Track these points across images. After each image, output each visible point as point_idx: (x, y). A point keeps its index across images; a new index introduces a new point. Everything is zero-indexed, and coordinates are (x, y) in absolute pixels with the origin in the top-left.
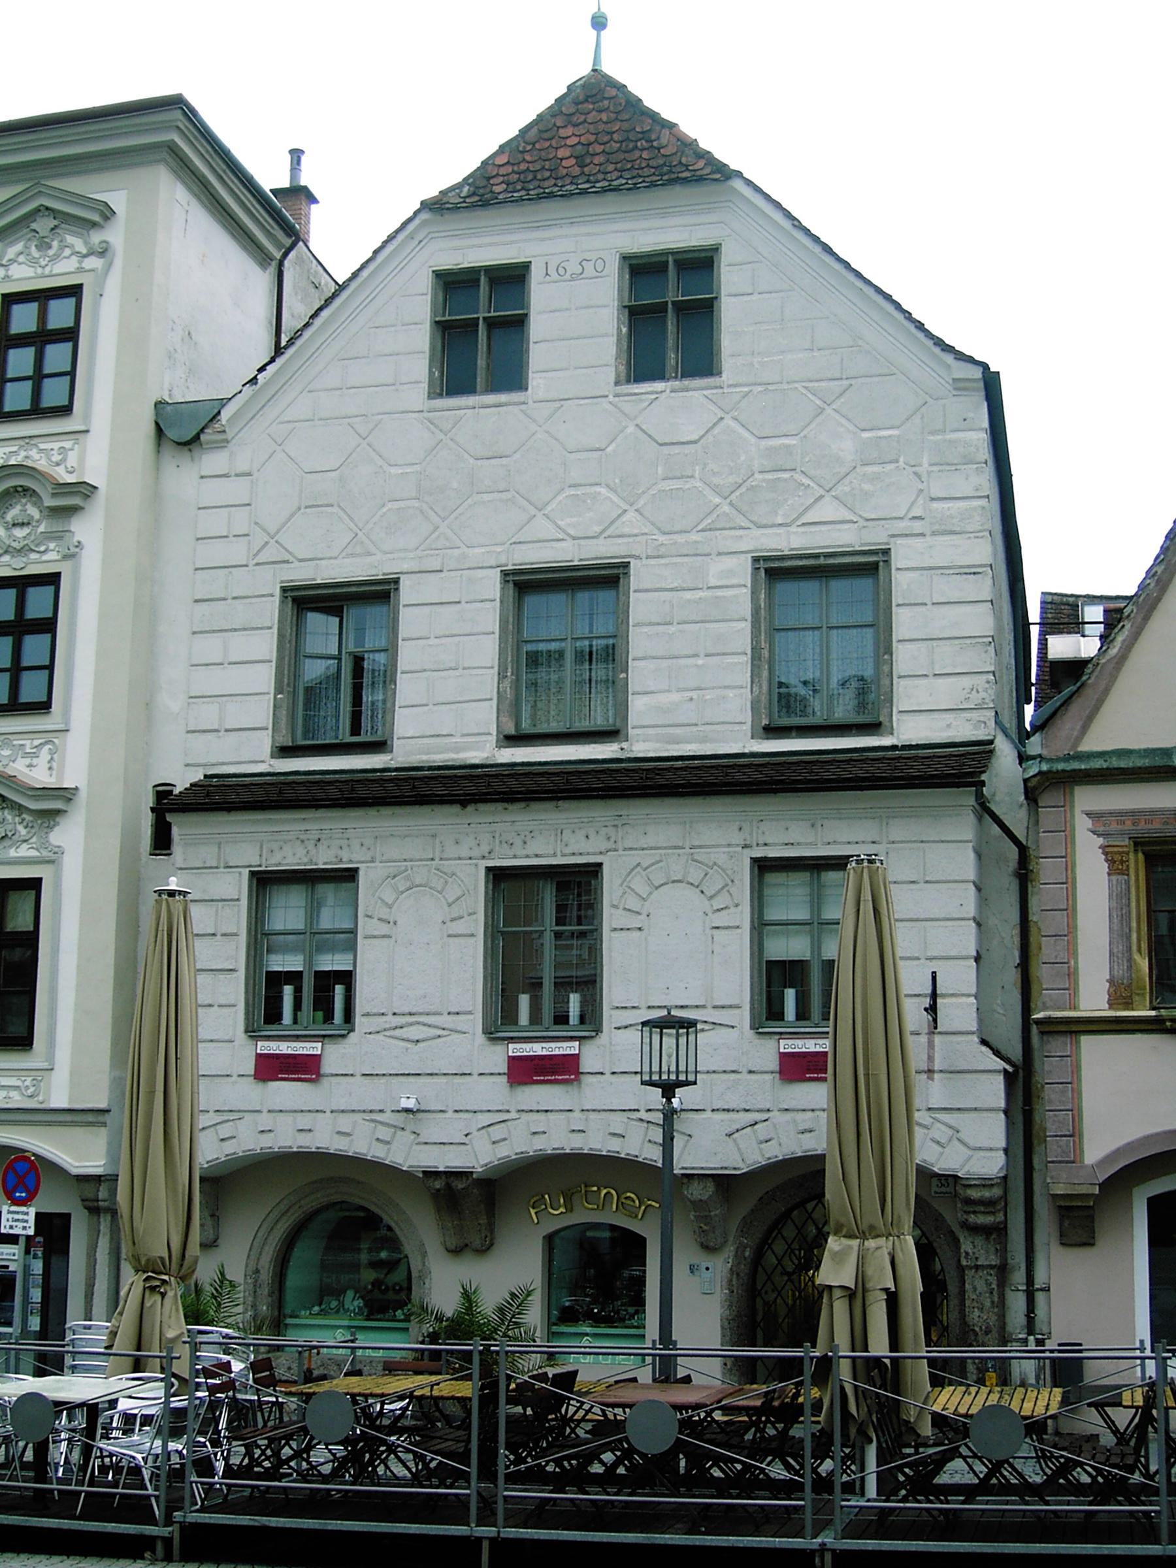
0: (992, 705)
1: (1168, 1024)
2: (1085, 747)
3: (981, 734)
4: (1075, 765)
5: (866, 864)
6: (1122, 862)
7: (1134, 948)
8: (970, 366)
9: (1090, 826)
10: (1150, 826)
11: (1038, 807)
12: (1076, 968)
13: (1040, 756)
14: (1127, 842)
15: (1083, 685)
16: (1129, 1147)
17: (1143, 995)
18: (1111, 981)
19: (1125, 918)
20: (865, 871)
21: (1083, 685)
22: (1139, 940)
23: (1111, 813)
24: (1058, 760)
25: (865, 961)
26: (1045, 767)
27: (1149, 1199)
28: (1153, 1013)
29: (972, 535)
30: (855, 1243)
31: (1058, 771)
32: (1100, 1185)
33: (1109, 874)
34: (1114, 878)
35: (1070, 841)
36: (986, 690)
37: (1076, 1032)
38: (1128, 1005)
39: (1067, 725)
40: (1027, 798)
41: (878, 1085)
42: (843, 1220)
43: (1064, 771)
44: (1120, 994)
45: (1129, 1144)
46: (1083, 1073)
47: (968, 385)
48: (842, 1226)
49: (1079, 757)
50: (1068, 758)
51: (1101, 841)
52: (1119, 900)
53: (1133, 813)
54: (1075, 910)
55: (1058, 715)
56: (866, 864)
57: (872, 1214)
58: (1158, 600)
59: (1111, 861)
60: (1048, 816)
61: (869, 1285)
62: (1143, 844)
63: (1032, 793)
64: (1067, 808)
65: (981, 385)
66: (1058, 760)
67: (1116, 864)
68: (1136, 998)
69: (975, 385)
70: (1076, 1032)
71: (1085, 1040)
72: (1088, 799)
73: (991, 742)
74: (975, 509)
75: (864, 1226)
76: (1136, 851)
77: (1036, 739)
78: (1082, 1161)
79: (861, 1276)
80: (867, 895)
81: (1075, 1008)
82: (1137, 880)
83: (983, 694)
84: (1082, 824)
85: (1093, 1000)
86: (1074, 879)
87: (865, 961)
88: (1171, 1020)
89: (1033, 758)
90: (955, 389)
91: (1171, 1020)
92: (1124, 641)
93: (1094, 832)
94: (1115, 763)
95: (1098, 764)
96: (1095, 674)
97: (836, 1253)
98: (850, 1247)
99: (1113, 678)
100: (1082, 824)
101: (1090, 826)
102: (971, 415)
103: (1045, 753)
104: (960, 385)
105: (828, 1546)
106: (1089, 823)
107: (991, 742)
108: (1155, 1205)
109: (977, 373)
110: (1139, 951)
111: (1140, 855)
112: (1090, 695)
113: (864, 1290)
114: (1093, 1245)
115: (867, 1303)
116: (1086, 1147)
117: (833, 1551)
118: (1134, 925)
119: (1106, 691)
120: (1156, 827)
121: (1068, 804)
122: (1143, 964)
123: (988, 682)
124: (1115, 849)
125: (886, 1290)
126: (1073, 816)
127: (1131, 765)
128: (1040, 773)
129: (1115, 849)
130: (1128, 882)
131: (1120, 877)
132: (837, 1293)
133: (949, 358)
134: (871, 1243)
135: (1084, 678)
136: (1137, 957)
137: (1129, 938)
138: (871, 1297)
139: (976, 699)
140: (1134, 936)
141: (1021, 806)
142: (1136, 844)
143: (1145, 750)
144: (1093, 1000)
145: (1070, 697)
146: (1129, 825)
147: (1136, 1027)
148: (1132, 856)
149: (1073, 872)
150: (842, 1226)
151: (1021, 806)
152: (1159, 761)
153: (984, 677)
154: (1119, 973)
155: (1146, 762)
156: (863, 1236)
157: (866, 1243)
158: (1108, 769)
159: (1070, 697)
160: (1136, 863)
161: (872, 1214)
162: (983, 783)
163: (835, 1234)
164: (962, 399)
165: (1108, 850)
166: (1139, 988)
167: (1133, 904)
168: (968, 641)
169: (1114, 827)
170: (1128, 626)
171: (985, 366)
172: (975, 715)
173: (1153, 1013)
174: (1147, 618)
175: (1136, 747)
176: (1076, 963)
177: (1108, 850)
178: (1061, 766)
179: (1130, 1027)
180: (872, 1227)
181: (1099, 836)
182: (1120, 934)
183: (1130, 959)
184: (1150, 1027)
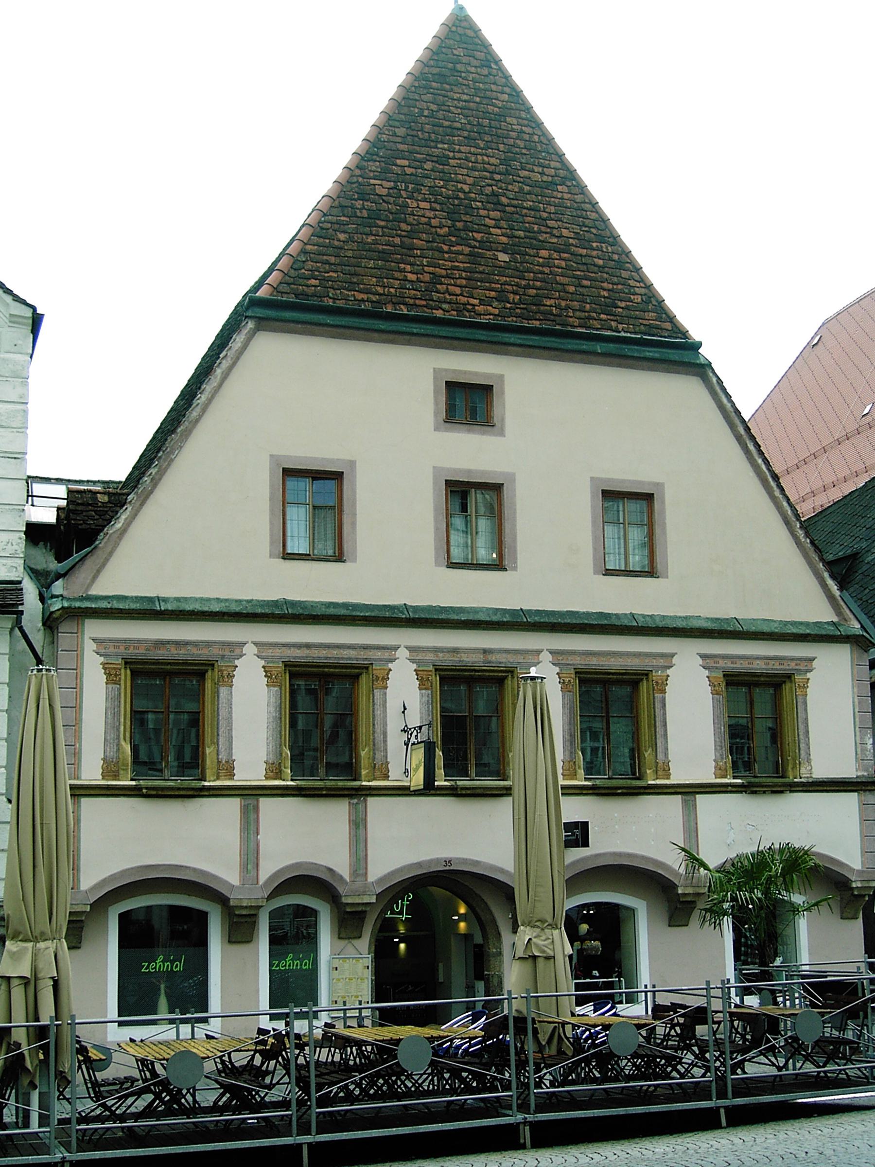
0: (22, 556)
1: (144, 791)
2: (94, 591)
3: (13, 576)
4: (87, 604)
5: (44, 672)
6: (116, 675)
7: (122, 736)
8: (23, 306)
9: (95, 649)
10: (137, 651)
11: (58, 632)
12: (80, 749)
13: (61, 596)
14: (120, 661)
15: (95, 547)
16: (113, 877)
17: (127, 769)
18: (104, 759)
19: (116, 715)
20: (44, 677)
21: (95, 547)
22: (125, 731)
23: (110, 640)
24: (75, 599)
25: (43, 742)
26: (66, 604)
27: (120, 915)
28: (133, 783)
29: (15, 430)
30: (30, 945)
31: (75, 608)
32: (91, 905)
33: (107, 684)
34: (110, 686)
35: (80, 658)
36: (18, 544)
37: (78, 795)
38: (116, 777)
39: (83, 574)
40: (44, 624)
41: (49, 831)
42: (21, 929)
43: (79, 608)
44: (111, 768)
45: (112, 875)
46: (82, 824)
47: (20, 320)
48: (20, 933)
49: (89, 598)
50: (82, 599)
51: (102, 659)
52: (113, 701)
53: (125, 641)
54: (81, 707)
55: (77, 567)
56: (44, 672)
57: (43, 924)
58: (151, 492)
59: (108, 675)
60: (65, 639)
61: (40, 976)
62: (131, 663)
63: (50, 623)
64: (79, 634)
65: (30, 321)
66: (75, 599)
67: (112, 676)
68: (121, 772)
69: (25, 321)
70: (78, 795)
71: (370, 800)
72: (94, 629)
73: (20, 582)
74: (18, 411)
75: (37, 933)
76: (126, 668)
77: (59, 583)
78: (78, 888)
79: (35, 970)
80: (45, 695)
81: (78, 778)
82: (126, 688)
83: (15, 547)
84: (90, 647)
85: (91, 773)
86: (82, 685)
87: (43, 742)
88: (146, 788)
89: (57, 596)
90: (10, 322)
91: (146, 788)
92: (126, 519)
93: (98, 653)
94: (116, 605)
95: (104, 605)
96: (105, 540)
97: (14, 953)
98: (26, 948)
99: (116, 545)
100: (90, 647)
101: (95, 649)
102: (20, 342)
103: (65, 594)
104: (14, 319)
105: (67, 1159)
106: (94, 646)
107: (20, 582)
108: (125, 919)
109: (29, 313)
110: (125, 739)
111: (128, 672)
112: (100, 555)
113: (36, 979)
114: (79, 948)
115: (39, 988)
116: (81, 880)
117: (71, 1162)
118: (122, 720)
119: (111, 554)
120: (140, 652)
121: (80, 632)
122: (127, 748)
123: (20, 538)
124: (112, 666)
125: (53, 978)
126: (83, 642)
127: (127, 607)
128: (63, 608)
129: (112, 666)
130: (119, 690)
131: (114, 686)
132: (14, 982)
133: (8, 299)
134: (42, 945)
135: (97, 542)
136: (123, 743)
137: (118, 730)
138: (41, 984)
139: (10, 550)
140: (122, 728)
141: (39, 630)
142: (126, 663)
143: (136, 597)
144: (91, 773)
145: (86, 556)
146: (122, 650)
147: (394, 792)
148: (123, 671)
149: (82, 681)
150: (20, 933)
151: (39, 630)
152: (146, 606)
153: (18, 535)
154: (111, 754)
155: (133, 606)
156: (36, 940)
157: (38, 945)
158: (111, 609)
159: (86, 556)
160: (125, 675)
161: (43, 924)
162: (22, 612)
163: (12, 939)
164: (12, 329)
165: (106, 666)
166: (123, 765)
167: (122, 706)
168: (7, 507)
169: (112, 650)
170: (129, 509)
171: (34, 308)
172: (9, 562)
173: (133, 783)
174: (142, 504)
175: (130, 594)
176: (80, 745)
177: (106, 666)
178: (78, 604)
179: (269, 792)
180: (42, 933)
181: (101, 655)
182: (111, 726)
183: (118, 745)
184: (133, 793)
